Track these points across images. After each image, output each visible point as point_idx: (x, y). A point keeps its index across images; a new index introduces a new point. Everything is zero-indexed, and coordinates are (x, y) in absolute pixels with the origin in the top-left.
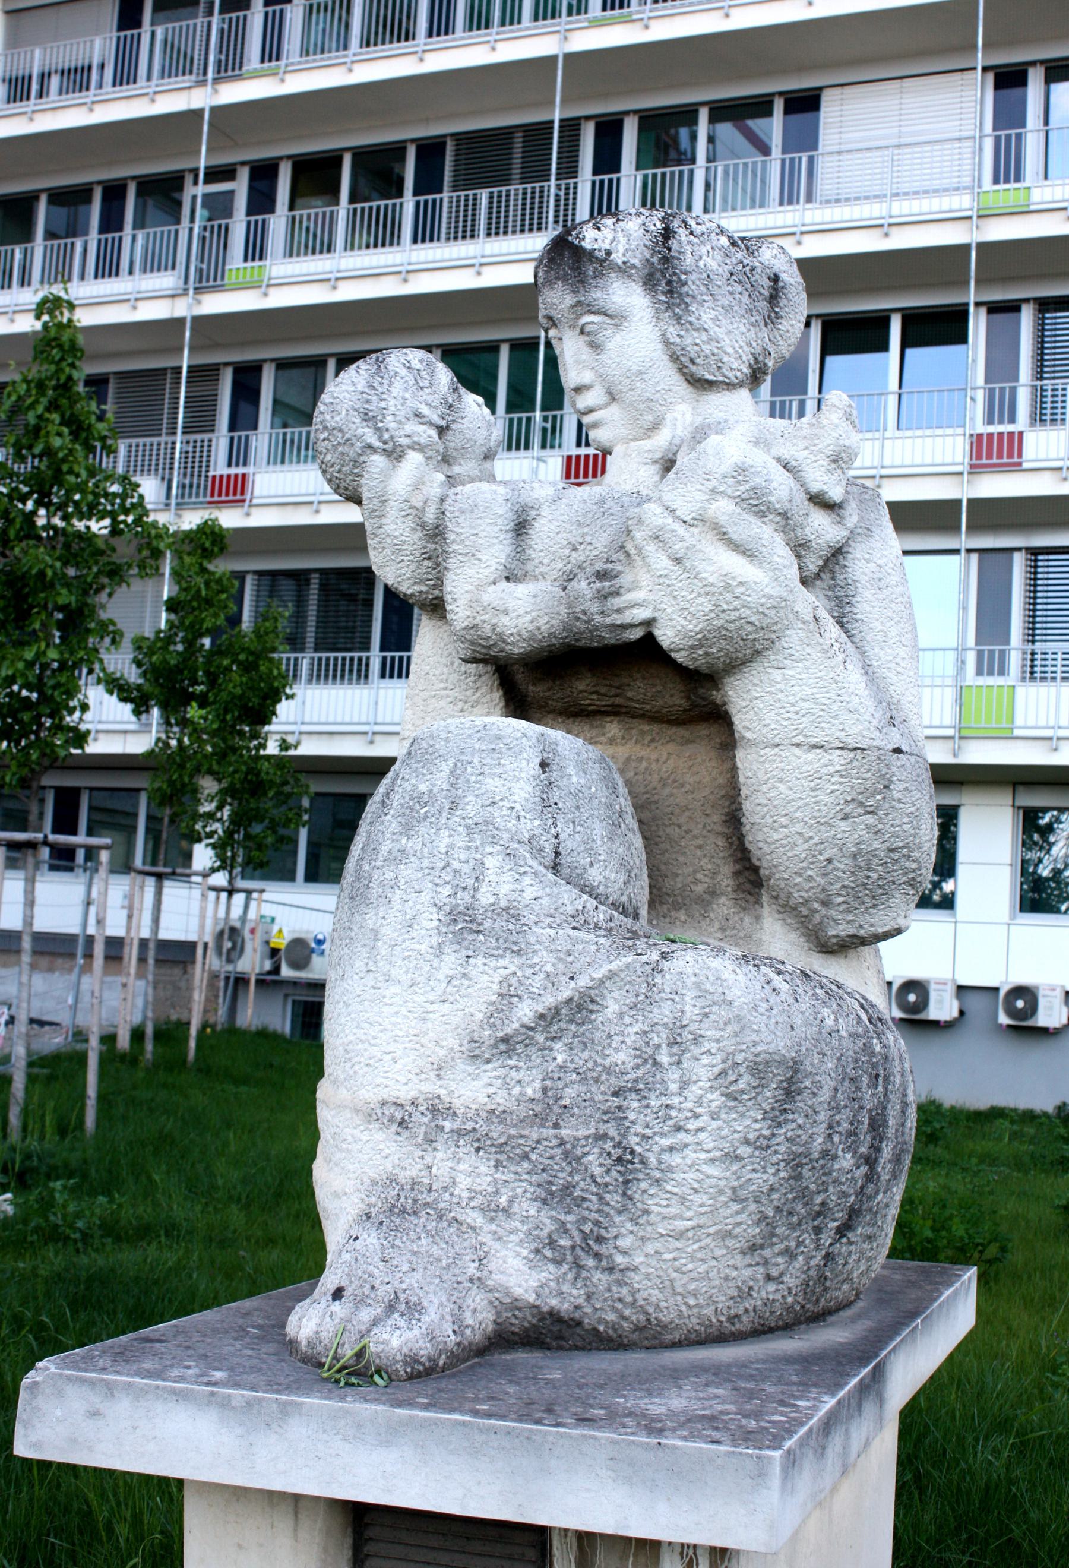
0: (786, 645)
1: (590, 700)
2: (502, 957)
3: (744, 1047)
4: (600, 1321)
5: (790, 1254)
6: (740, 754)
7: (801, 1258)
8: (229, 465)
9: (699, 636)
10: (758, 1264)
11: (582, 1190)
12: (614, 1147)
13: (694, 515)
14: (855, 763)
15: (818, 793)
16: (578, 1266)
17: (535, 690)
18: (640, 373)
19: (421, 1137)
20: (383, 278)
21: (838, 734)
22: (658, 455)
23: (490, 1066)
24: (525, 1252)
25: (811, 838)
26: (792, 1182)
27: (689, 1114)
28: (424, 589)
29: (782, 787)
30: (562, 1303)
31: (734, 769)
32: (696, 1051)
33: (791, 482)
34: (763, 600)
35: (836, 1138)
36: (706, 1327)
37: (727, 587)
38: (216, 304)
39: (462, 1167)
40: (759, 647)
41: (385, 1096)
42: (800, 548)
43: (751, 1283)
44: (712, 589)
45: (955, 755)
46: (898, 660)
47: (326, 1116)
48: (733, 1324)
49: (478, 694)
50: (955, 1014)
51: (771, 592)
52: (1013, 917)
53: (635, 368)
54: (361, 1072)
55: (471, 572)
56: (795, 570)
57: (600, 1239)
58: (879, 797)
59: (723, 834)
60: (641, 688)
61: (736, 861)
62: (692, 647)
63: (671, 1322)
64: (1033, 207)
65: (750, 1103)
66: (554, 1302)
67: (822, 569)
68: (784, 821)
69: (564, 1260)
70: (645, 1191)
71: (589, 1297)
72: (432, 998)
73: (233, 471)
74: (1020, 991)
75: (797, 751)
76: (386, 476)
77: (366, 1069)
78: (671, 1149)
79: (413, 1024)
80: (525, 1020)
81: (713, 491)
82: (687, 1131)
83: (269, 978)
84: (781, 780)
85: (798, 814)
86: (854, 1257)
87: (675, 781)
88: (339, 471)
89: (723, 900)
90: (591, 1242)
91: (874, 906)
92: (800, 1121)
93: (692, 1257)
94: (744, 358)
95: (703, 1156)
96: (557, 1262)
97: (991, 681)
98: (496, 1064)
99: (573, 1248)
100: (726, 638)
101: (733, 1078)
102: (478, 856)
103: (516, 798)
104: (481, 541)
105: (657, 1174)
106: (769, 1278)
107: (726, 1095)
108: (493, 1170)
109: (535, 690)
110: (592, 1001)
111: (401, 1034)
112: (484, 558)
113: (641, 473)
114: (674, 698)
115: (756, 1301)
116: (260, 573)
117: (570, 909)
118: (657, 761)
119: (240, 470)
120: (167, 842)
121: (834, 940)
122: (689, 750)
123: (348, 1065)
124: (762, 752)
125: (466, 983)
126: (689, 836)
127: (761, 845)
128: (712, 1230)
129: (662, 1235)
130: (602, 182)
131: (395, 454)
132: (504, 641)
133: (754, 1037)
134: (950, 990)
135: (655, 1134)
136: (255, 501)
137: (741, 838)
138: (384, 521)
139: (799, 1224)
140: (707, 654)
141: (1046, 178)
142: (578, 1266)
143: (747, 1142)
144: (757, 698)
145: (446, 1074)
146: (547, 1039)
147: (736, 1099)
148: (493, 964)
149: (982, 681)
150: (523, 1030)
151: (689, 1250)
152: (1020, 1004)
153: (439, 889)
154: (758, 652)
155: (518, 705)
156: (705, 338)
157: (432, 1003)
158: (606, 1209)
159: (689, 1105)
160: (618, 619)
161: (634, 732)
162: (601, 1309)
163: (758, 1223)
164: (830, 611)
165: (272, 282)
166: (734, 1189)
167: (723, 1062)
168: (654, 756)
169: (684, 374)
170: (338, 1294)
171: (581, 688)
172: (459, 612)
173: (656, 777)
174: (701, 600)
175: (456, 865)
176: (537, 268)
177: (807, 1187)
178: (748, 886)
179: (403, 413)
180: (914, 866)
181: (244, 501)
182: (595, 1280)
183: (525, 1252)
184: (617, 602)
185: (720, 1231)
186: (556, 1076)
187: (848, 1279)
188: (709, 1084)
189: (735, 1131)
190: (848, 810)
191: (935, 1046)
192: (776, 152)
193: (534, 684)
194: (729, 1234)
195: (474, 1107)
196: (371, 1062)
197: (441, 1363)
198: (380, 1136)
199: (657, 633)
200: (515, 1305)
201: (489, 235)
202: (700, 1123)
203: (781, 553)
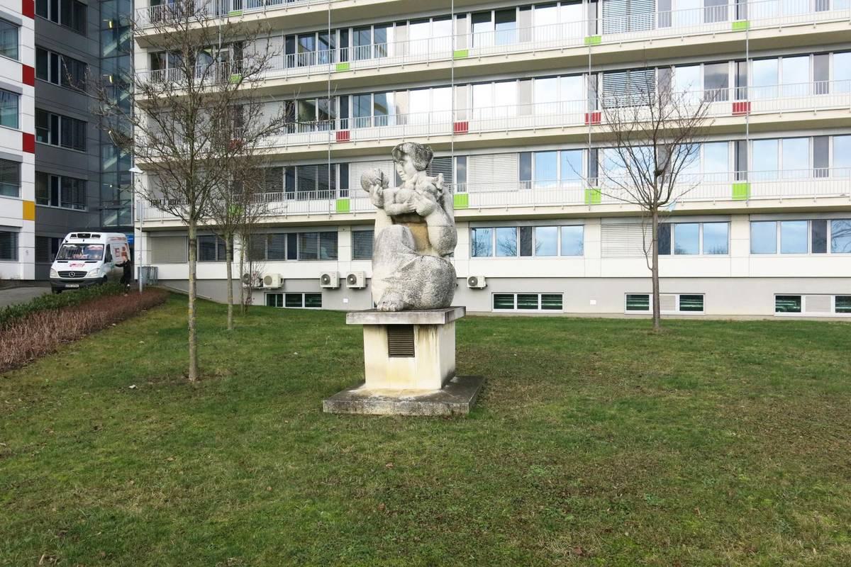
1: (405, 221)
8: (342, 128)
42: (436, 197)
52: (470, 258)
60: (413, 219)
73: (343, 130)
74: (473, 278)
114: (418, 220)
119: (345, 130)
131: (375, 185)
141: (738, 19)
149: (459, 193)
152: (473, 281)
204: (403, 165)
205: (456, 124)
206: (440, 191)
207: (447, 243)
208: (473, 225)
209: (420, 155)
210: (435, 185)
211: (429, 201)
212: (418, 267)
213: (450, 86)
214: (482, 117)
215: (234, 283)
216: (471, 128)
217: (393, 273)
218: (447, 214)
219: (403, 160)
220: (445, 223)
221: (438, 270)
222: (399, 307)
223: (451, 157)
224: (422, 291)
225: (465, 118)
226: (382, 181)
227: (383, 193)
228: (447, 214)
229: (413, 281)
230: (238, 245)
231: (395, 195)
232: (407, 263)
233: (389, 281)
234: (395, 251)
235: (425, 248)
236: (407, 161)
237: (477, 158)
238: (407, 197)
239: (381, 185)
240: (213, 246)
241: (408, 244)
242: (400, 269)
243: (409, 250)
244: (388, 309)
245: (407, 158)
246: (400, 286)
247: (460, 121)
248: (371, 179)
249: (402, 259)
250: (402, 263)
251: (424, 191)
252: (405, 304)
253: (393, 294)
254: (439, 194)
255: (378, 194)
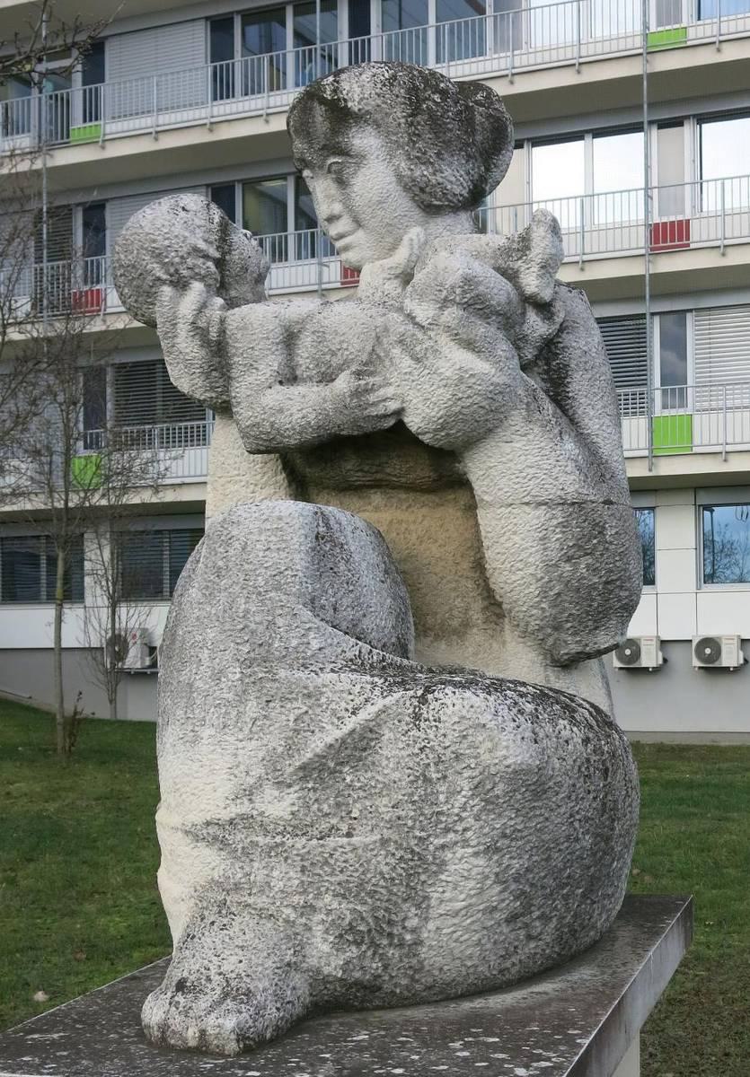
0: (513, 423)
1: (357, 477)
2: (296, 699)
3: (497, 761)
4: (396, 985)
5: (545, 918)
6: (480, 513)
7: (554, 920)
9: (441, 421)
10: (520, 928)
11: (374, 885)
12: (397, 849)
13: (430, 320)
14: (575, 515)
15: (546, 541)
16: (374, 945)
17: (310, 472)
18: (380, 202)
19: (240, 851)
20: (192, 130)
21: (559, 493)
22: (399, 271)
23: (292, 790)
24: (331, 938)
25: (542, 578)
26: (543, 863)
27: (456, 818)
28: (214, 395)
29: (516, 538)
30: (364, 974)
31: (477, 525)
32: (459, 767)
33: (509, 286)
34: (492, 388)
35: (577, 824)
36: (483, 980)
37: (461, 379)
38: (64, 158)
39: (275, 873)
40: (491, 426)
41: (209, 819)
42: (518, 342)
43: (516, 943)
44: (450, 382)
45: (650, 470)
46: (604, 428)
47: (163, 835)
48: (504, 975)
49: (265, 478)
50: (660, 662)
51: (498, 381)
52: (699, 588)
53: (376, 198)
54: (188, 800)
55: (250, 379)
56: (516, 360)
57: (390, 923)
58: (595, 541)
59: (472, 578)
60: (396, 467)
61: (483, 599)
62: (435, 430)
63: (453, 980)
64: (689, 43)
65: (505, 805)
66: (357, 974)
67: (537, 357)
68: (520, 565)
69: (362, 942)
70: (424, 882)
71: (385, 967)
72: (240, 737)
74: (707, 642)
75: (526, 508)
76: (175, 303)
77: (192, 797)
78: (443, 847)
79: (226, 759)
80: (318, 750)
81: (445, 300)
82: (456, 832)
83: (149, 671)
84: (515, 533)
85: (530, 560)
86: (596, 912)
87: (429, 539)
88: (136, 301)
89: (475, 630)
90: (384, 926)
91: (596, 628)
92: (546, 815)
93: (467, 930)
94: (465, 185)
95: (470, 850)
96: (358, 944)
97: (673, 412)
98: (297, 788)
99: (369, 931)
100: (463, 421)
101: (489, 787)
102: (270, 618)
103: (298, 567)
104: (257, 353)
105: (434, 868)
106: (530, 937)
107: (485, 801)
108: (299, 875)
109: (310, 472)
110: (371, 731)
111: (217, 767)
112: (261, 367)
113: (386, 286)
114: (422, 471)
115: (522, 955)
116: (121, 367)
117: (350, 655)
118: (414, 522)
120: (156, 489)
121: (566, 657)
122: (439, 513)
123: (178, 794)
124: (499, 511)
125: (268, 723)
126: (444, 581)
127: (502, 585)
128: (481, 907)
129: (441, 915)
130: (356, 42)
131: (180, 284)
132: (282, 435)
133: (504, 752)
134: (654, 643)
135: (429, 836)
136: (109, 311)
137: (486, 580)
138: (178, 340)
139: (551, 894)
140: (448, 435)
141: (699, 19)
142: (374, 945)
143: (504, 836)
144: (491, 468)
145: (256, 798)
146: (337, 764)
147: (493, 803)
148: (289, 706)
149: (666, 413)
150: (316, 759)
151: (464, 924)
152: (708, 651)
153: (240, 647)
154: (490, 430)
155: (300, 487)
156: (431, 170)
157: (241, 741)
158: (394, 898)
159: (456, 811)
160: (374, 411)
161: (394, 500)
162: (397, 976)
163: (517, 898)
164: (547, 392)
165: (107, 137)
166: (497, 875)
167: (481, 774)
168: (412, 518)
169: (415, 201)
170: (181, 986)
171: (349, 467)
172: (244, 412)
173: (414, 536)
174: (441, 391)
175: (253, 626)
176: (289, 118)
177: (555, 866)
178: (494, 618)
179: (185, 249)
180: (627, 593)
181: (100, 310)
182: (390, 955)
183: (331, 938)
184: (372, 398)
185: (488, 907)
186: (346, 793)
187: (594, 927)
188: (471, 793)
189: (494, 829)
190: (570, 553)
191: (647, 683)
192: (489, 11)
193: (310, 467)
194: (495, 908)
195: (282, 823)
196: (196, 791)
197: (268, 1035)
198: (207, 851)
199: (406, 420)
200: (326, 980)
201: (272, 90)
202: (464, 825)
203: (503, 347)
204: (342, 182)
205: (657, 225)
206: (544, 308)
207: (577, 590)
208: (704, 499)
209: (436, 124)
210: (511, 276)
211: (481, 366)
212: (394, 755)
213: (637, 128)
214: (728, 206)
215: (67, 660)
216: (697, 234)
217: (250, 793)
218: (583, 439)
219: (344, 153)
220: (570, 483)
221: (516, 776)
222: (272, 1014)
223: (643, 316)
224: (422, 903)
225: (683, 212)
226: (220, 263)
227: (222, 332)
228: (583, 439)
229: (364, 844)
230: (98, 555)
231: (290, 339)
232: (333, 734)
233: (223, 844)
234: (260, 659)
235: (467, 624)
236: (361, 157)
237: (716, 315)
238: (356, 347)
239: (222, 288)
240: (33, 560)
241: (347, 614)
242: (289, 767)
243: (350, 646)
244: (192, 1036)
245: (364, 140)
246: (284, 876)
247: (665, 220)
248: (158, 255)
249: (300, 706)
250: (300, 729)
251: (445, 303)
252: (318, 980)
253: (243, 926)
254: (536, 326)
255: (200, 332)
